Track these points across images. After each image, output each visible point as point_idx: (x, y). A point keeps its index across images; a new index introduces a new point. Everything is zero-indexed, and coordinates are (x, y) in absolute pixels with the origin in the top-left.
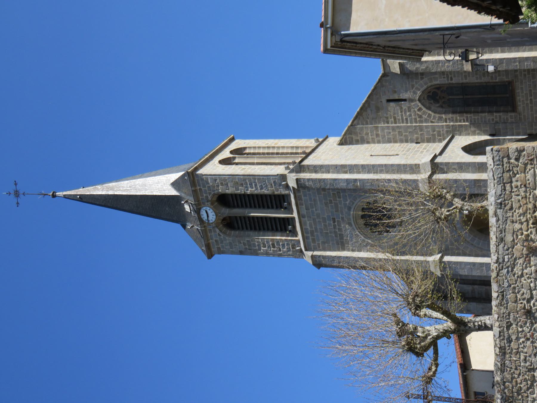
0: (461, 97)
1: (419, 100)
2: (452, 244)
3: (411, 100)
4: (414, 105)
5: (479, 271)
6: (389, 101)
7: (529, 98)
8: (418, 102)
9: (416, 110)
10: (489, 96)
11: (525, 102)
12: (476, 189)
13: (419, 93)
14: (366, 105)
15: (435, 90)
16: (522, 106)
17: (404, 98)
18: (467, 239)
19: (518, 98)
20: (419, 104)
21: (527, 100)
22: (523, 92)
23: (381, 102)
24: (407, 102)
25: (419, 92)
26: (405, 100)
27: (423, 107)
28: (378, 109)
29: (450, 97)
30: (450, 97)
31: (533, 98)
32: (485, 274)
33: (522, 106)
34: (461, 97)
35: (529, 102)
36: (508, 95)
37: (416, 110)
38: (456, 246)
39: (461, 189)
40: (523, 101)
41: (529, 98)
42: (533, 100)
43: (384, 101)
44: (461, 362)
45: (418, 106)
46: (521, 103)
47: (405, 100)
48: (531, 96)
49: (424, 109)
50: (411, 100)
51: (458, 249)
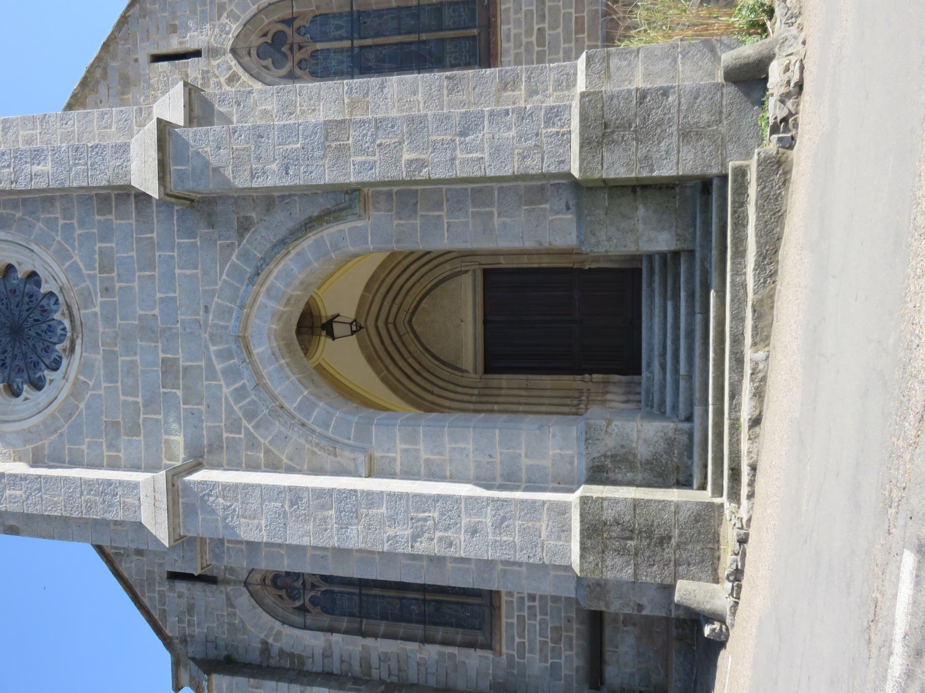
0: (346, 44)
1: (233, 51)
2: (235, 426)
3: (214, 52)
4: (218, 66)
5: (310, 527)
6: (157, 58)
7: (536, 27)
8: (230, 56)
9: (222, 80)
10: (424, 37)
11: (524, 40)
12: (327, 162)
13: (235, 28)
14: (98, 73)
15: (281, 27)
16: (512, 52)
17: (192, 46)
18: (287, 405)
19: (504, 27)
20: (233, 63)
21: (529, 32)
22: (518, 10)
23: (136, 60)
24: (202, 60)
25: (234, 27)
26: (197, 53)
27: (240, 71)
28: (126, 83)
29: (319, 46)
30: (319, 46)
31: (546, 25)
32: (335, 542)
33: (512, 52)
34: (346, 44)
35: (534, 39)
36: (475, 31)
37: (222, 80)
38: (249, 434)
39: (274, 166)
40: (517, 36)
41: (536, 27)
42: (547, 32)
43: (143, 58)
44: (638, 418)
45: (230, 68)
46: (511, 45)
47: (197, 53)
48: (542, 18)
49: (244, 77)
50: (214, 52)
51: (253, 444)
